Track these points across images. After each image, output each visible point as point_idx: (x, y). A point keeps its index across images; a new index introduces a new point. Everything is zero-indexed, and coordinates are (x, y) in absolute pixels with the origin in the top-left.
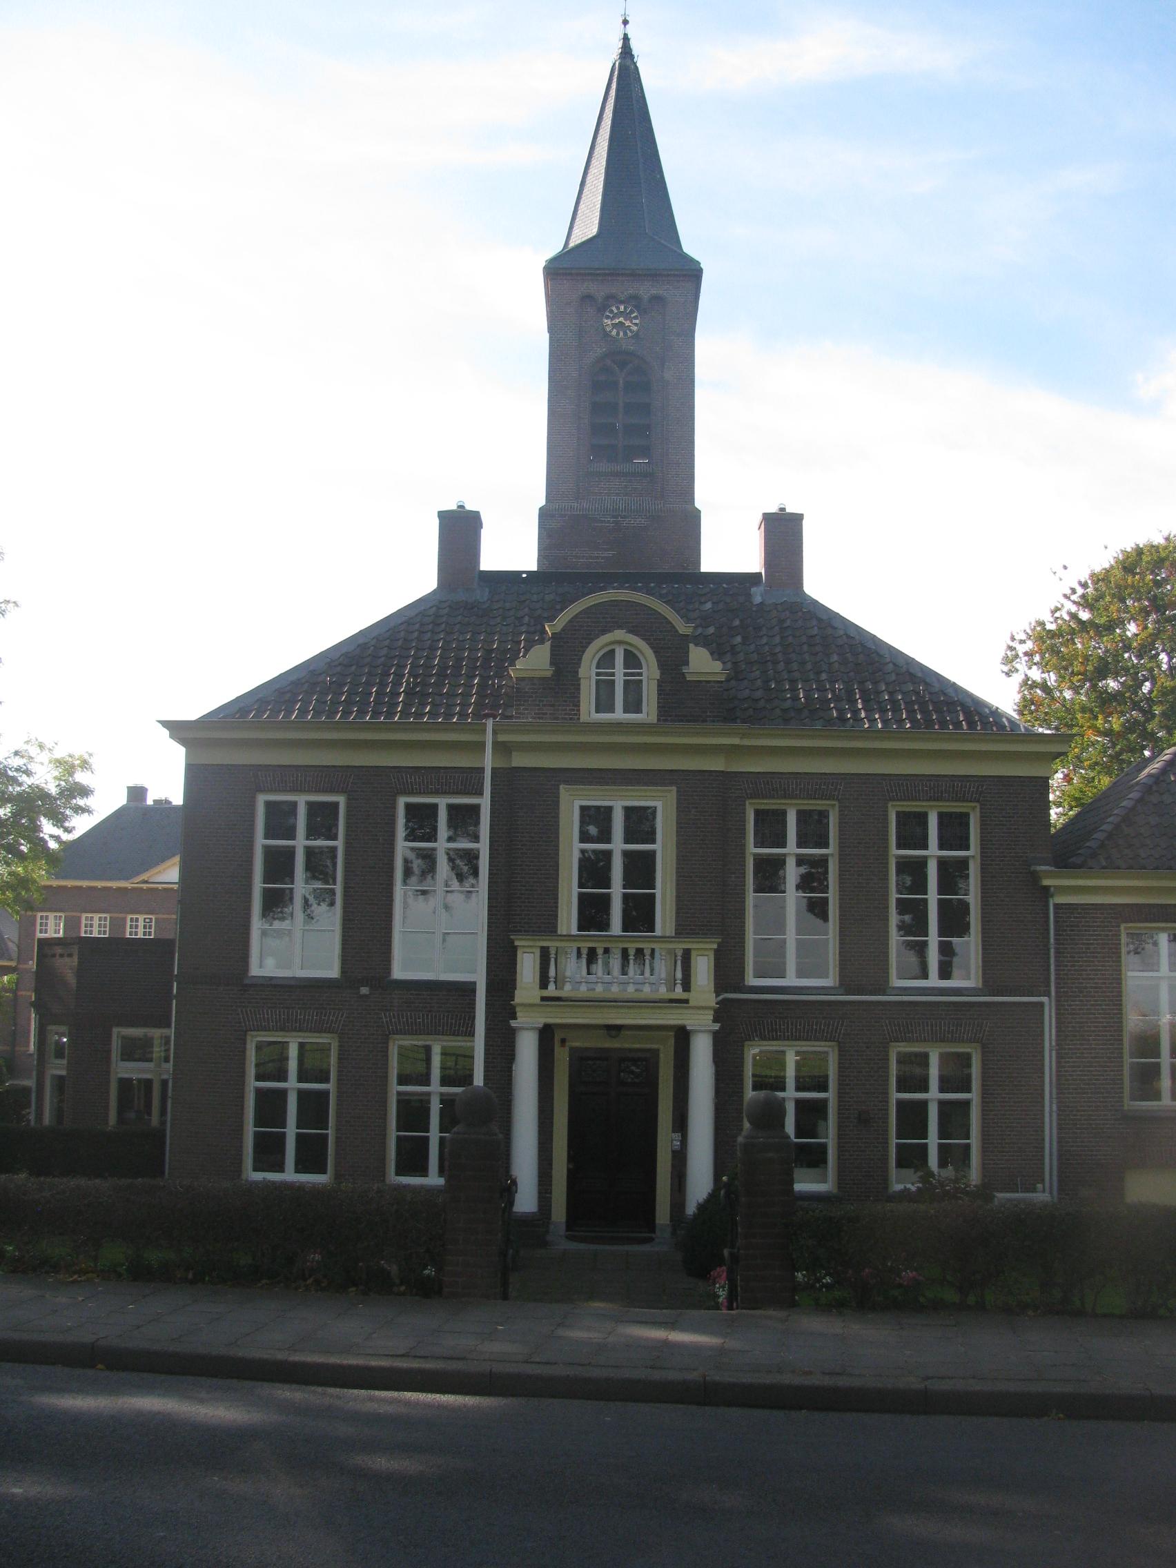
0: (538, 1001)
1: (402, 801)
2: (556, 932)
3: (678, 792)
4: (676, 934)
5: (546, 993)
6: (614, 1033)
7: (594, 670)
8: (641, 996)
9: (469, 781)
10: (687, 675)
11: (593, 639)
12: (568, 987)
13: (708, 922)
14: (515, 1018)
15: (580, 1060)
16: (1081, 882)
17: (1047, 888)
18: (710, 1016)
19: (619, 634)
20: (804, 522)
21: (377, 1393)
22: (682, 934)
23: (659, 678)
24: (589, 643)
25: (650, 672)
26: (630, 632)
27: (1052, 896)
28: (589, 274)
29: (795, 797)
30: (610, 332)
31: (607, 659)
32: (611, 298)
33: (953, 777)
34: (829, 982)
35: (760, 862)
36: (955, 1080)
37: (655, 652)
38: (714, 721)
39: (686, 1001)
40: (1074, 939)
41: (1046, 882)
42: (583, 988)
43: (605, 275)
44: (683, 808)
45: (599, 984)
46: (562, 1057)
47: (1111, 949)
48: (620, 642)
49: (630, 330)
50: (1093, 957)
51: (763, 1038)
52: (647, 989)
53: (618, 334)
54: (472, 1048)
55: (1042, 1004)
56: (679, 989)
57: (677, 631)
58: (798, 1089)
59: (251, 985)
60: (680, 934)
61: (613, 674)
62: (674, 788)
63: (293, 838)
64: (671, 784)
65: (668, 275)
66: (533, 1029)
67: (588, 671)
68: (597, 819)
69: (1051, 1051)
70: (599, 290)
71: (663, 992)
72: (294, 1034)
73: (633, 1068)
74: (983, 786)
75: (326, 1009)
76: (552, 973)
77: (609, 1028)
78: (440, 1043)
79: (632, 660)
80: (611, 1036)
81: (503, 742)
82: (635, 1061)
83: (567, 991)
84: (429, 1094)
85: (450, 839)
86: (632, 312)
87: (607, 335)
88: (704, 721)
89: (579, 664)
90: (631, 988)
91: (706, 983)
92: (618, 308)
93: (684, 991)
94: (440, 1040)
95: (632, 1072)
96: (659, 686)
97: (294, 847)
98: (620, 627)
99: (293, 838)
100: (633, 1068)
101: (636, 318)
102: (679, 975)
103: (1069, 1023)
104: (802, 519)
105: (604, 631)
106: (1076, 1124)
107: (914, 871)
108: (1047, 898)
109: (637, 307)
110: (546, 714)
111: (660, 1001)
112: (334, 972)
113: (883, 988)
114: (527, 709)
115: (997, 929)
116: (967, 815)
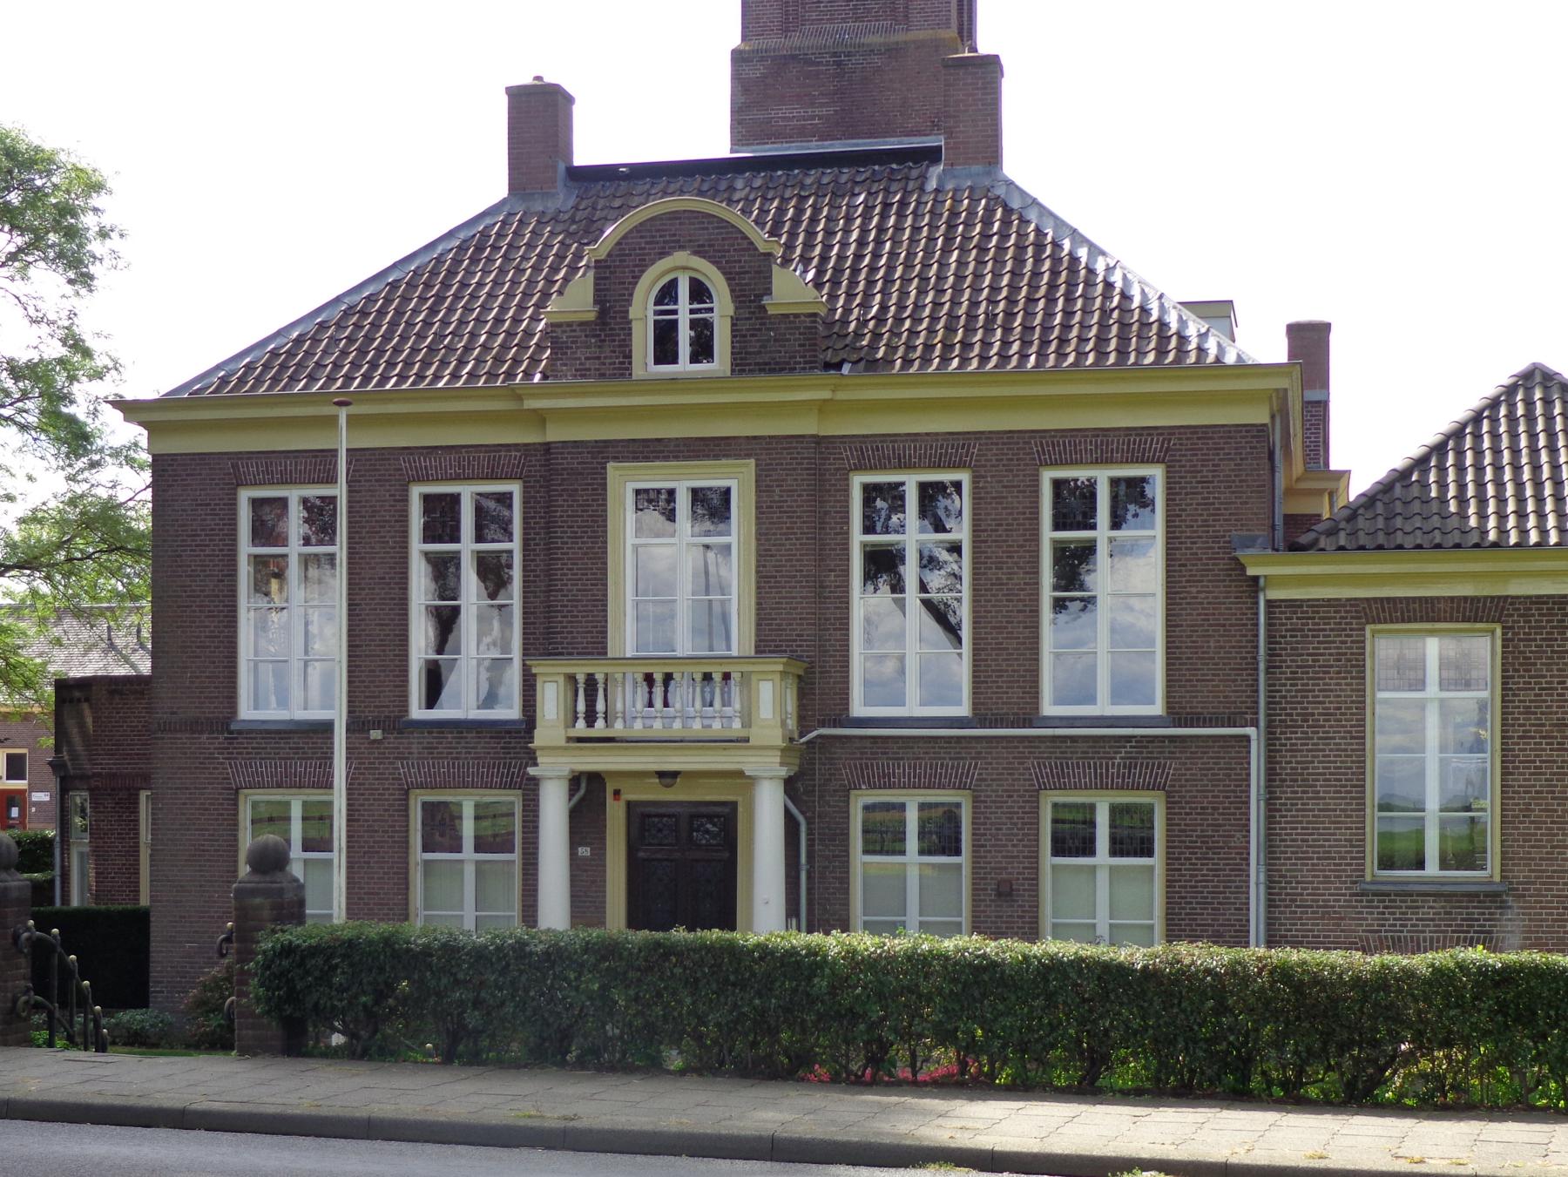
0: (563, 743)
1: (416, 492)
2: (606, 653)
3: (757, 465)
4: (756, 652)
5: (573, 733)
6: (668, 781)
7: (651, 308)
8: (649, 734)
9: (319, 465)
11: (647, 266)
12: (619, 725)
13: (797, 635)
14: (536, 764)
15: (642, 820)
17: (1256, 579)
18: (776, 759)
19: (681, 257)
22: (764, 652)
23: (732, 313)
24: (643, 271)
26: (696, 253)
27: (1264, 589)
31: (668, 293)
33: (1129, 431)
34: (963, 710)
35: (1061, 551)
37: (728, 279)
38: (804, 369)
39: (747, 740)
40: (1297, 649)
41: (1251, 572)
42: (638, 725)
44: (763, 486)
45: (659, 720)
46: (616, 817)
47: (1350, 660)
48: (685, 268)
50: (1325, 673)
51: (872, 786)
52: (658, 724)
54: (330, 804)
55: (1247, 738)
56: (581, 723)
57: (756, 249)
58: (478, 849)
59: (240, 732)
60: (762, 652)
62: (752, 462)
63: (457, 539)
64: (748, 456)
66: (559, 778)
67: (643, 313)
69: (1258, 801)
73: (709, 826)
74: (1170, 440)
76: (600, 706)
77: (661, 775)
79: (699, 292)
80: (667, 786)
81: (535, 411)
82: (710, 817)
83: (618, 728)
85: (307, 541)
88: (792, 370)
89: (629, 302)
90: (717, 725)
91: (771, 716)
94: (471, 795)
95: (707, 831)
96: (733, 325)
97: (459, 552)
98: (682, 248)
99: (457, 539)
100: (709, 826)
102: (581, 707)
103: (1287, 763)
105: (663, 254)
106: (1296, 900)
108: (1257, 592)
110: (589, 370)
113: (1030, 717)
114: (566, 365)
115: (1187, 636)
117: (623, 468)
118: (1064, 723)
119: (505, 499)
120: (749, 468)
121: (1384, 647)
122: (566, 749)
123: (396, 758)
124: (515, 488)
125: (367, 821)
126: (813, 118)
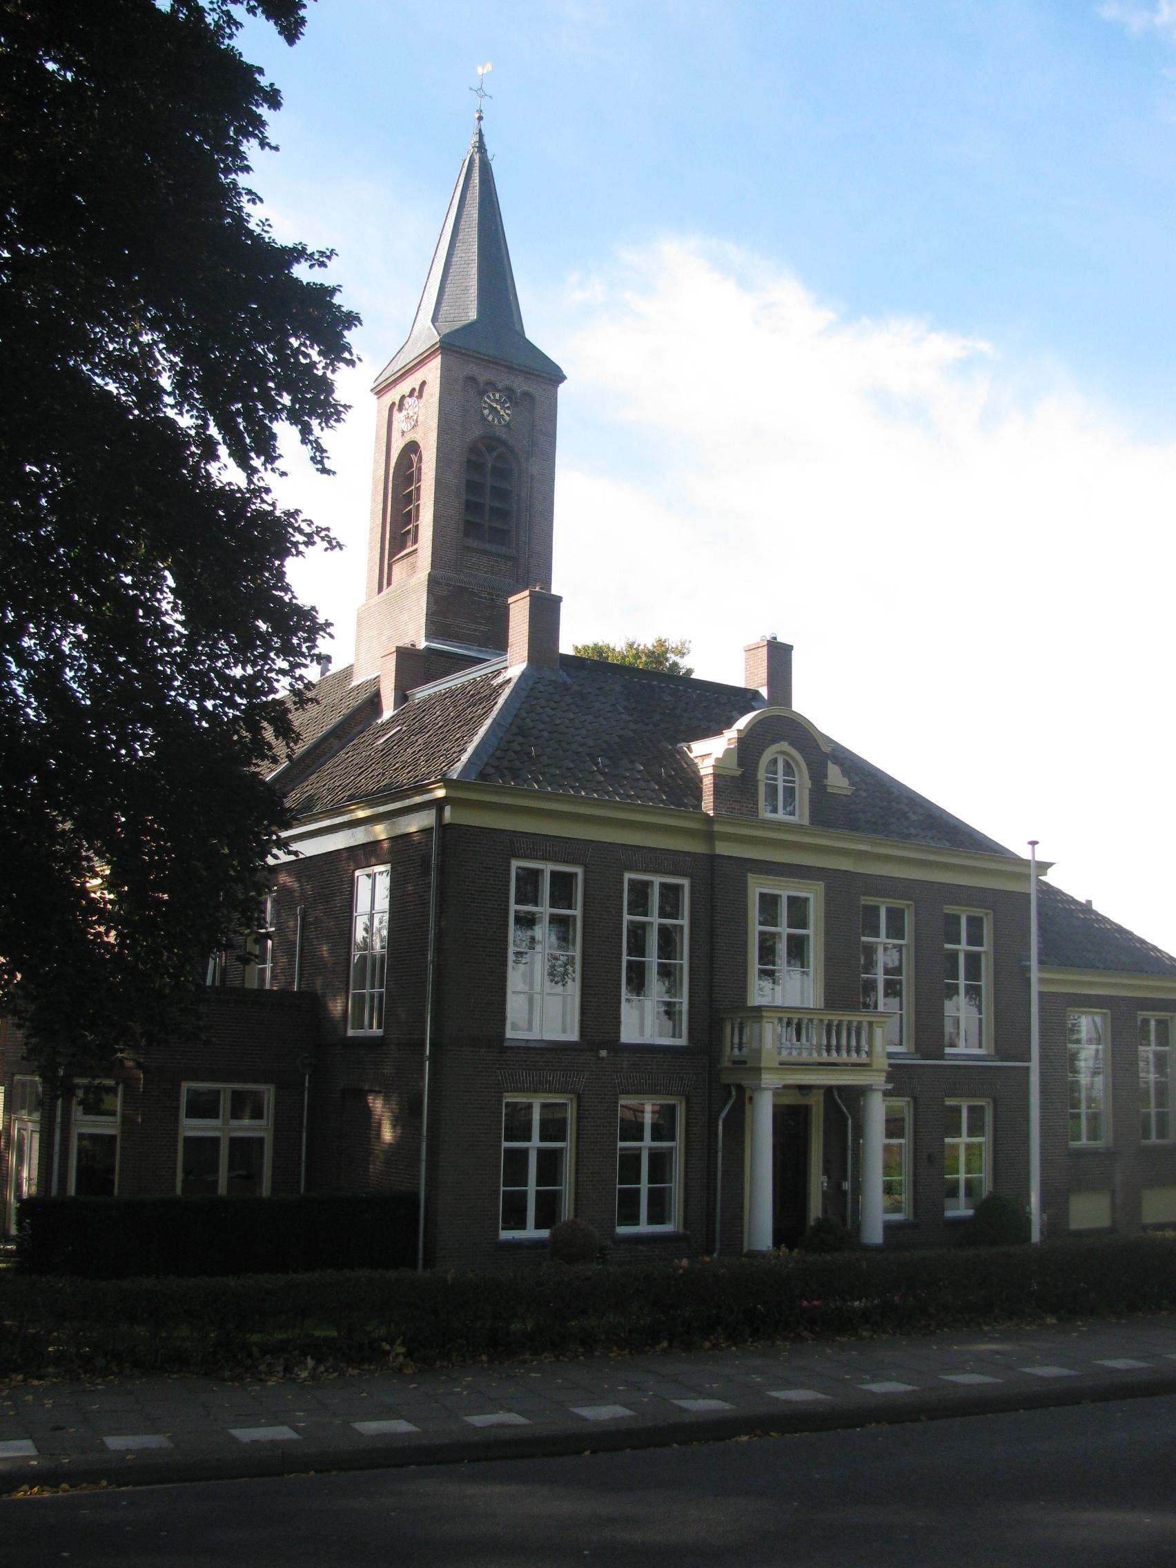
10: (828, 787)
16: (1070, 977)
19: (784, 746)
20: (562, 604)
21: (16, 1454)
25: (803, 782)
28: (476, 358)
29: (888, 896)
30: (488, 416)
32: (492, 385)
36: (553, 1129)
43: (489, 362)
49: (504, 420)
53: (493, 420)
61: (776, 779)
65: (539, 376)
68: (769, 903)
70: (483, 376)
71: (815, 1057)
72: (651, 1096)
75: (570, 1070)
78: (651, 1101)
79: (789, 770)
84: (640, 1149)
86: (505, 402)
87: (484, 418)
92: (494, 395)
93: (818, 1055)
101: (508, 408)
104: (561, 601)
107: (638, 932)
109: (510, 399)
111: (812, 1064)
112: (573, 1036)
113: (941, 1056)
116: (902, 911)
117: (776, 880)
118: (964, 1058)
119: (677, 889)
120: (820, 887)
121: (822, 1007)
122: (777, 1069)
123: (614, 1072)
124: (685, 882)
125: (593, 1118)
126: (475, 630)
